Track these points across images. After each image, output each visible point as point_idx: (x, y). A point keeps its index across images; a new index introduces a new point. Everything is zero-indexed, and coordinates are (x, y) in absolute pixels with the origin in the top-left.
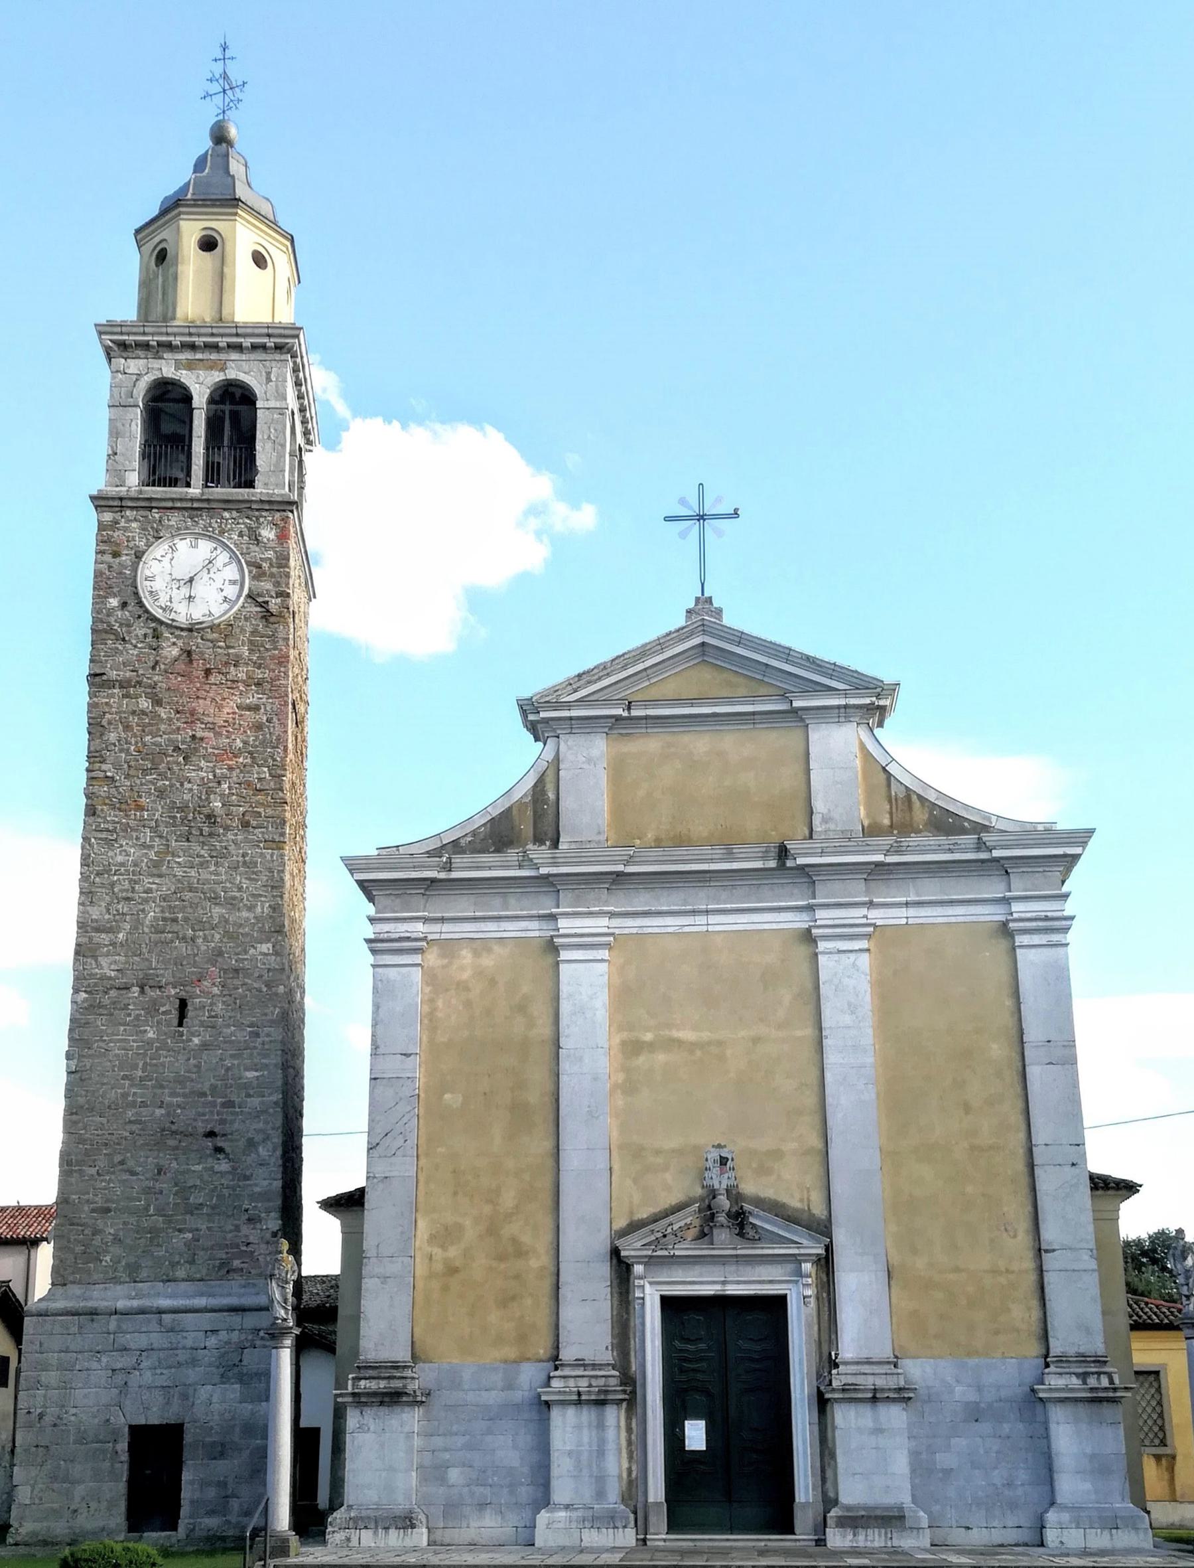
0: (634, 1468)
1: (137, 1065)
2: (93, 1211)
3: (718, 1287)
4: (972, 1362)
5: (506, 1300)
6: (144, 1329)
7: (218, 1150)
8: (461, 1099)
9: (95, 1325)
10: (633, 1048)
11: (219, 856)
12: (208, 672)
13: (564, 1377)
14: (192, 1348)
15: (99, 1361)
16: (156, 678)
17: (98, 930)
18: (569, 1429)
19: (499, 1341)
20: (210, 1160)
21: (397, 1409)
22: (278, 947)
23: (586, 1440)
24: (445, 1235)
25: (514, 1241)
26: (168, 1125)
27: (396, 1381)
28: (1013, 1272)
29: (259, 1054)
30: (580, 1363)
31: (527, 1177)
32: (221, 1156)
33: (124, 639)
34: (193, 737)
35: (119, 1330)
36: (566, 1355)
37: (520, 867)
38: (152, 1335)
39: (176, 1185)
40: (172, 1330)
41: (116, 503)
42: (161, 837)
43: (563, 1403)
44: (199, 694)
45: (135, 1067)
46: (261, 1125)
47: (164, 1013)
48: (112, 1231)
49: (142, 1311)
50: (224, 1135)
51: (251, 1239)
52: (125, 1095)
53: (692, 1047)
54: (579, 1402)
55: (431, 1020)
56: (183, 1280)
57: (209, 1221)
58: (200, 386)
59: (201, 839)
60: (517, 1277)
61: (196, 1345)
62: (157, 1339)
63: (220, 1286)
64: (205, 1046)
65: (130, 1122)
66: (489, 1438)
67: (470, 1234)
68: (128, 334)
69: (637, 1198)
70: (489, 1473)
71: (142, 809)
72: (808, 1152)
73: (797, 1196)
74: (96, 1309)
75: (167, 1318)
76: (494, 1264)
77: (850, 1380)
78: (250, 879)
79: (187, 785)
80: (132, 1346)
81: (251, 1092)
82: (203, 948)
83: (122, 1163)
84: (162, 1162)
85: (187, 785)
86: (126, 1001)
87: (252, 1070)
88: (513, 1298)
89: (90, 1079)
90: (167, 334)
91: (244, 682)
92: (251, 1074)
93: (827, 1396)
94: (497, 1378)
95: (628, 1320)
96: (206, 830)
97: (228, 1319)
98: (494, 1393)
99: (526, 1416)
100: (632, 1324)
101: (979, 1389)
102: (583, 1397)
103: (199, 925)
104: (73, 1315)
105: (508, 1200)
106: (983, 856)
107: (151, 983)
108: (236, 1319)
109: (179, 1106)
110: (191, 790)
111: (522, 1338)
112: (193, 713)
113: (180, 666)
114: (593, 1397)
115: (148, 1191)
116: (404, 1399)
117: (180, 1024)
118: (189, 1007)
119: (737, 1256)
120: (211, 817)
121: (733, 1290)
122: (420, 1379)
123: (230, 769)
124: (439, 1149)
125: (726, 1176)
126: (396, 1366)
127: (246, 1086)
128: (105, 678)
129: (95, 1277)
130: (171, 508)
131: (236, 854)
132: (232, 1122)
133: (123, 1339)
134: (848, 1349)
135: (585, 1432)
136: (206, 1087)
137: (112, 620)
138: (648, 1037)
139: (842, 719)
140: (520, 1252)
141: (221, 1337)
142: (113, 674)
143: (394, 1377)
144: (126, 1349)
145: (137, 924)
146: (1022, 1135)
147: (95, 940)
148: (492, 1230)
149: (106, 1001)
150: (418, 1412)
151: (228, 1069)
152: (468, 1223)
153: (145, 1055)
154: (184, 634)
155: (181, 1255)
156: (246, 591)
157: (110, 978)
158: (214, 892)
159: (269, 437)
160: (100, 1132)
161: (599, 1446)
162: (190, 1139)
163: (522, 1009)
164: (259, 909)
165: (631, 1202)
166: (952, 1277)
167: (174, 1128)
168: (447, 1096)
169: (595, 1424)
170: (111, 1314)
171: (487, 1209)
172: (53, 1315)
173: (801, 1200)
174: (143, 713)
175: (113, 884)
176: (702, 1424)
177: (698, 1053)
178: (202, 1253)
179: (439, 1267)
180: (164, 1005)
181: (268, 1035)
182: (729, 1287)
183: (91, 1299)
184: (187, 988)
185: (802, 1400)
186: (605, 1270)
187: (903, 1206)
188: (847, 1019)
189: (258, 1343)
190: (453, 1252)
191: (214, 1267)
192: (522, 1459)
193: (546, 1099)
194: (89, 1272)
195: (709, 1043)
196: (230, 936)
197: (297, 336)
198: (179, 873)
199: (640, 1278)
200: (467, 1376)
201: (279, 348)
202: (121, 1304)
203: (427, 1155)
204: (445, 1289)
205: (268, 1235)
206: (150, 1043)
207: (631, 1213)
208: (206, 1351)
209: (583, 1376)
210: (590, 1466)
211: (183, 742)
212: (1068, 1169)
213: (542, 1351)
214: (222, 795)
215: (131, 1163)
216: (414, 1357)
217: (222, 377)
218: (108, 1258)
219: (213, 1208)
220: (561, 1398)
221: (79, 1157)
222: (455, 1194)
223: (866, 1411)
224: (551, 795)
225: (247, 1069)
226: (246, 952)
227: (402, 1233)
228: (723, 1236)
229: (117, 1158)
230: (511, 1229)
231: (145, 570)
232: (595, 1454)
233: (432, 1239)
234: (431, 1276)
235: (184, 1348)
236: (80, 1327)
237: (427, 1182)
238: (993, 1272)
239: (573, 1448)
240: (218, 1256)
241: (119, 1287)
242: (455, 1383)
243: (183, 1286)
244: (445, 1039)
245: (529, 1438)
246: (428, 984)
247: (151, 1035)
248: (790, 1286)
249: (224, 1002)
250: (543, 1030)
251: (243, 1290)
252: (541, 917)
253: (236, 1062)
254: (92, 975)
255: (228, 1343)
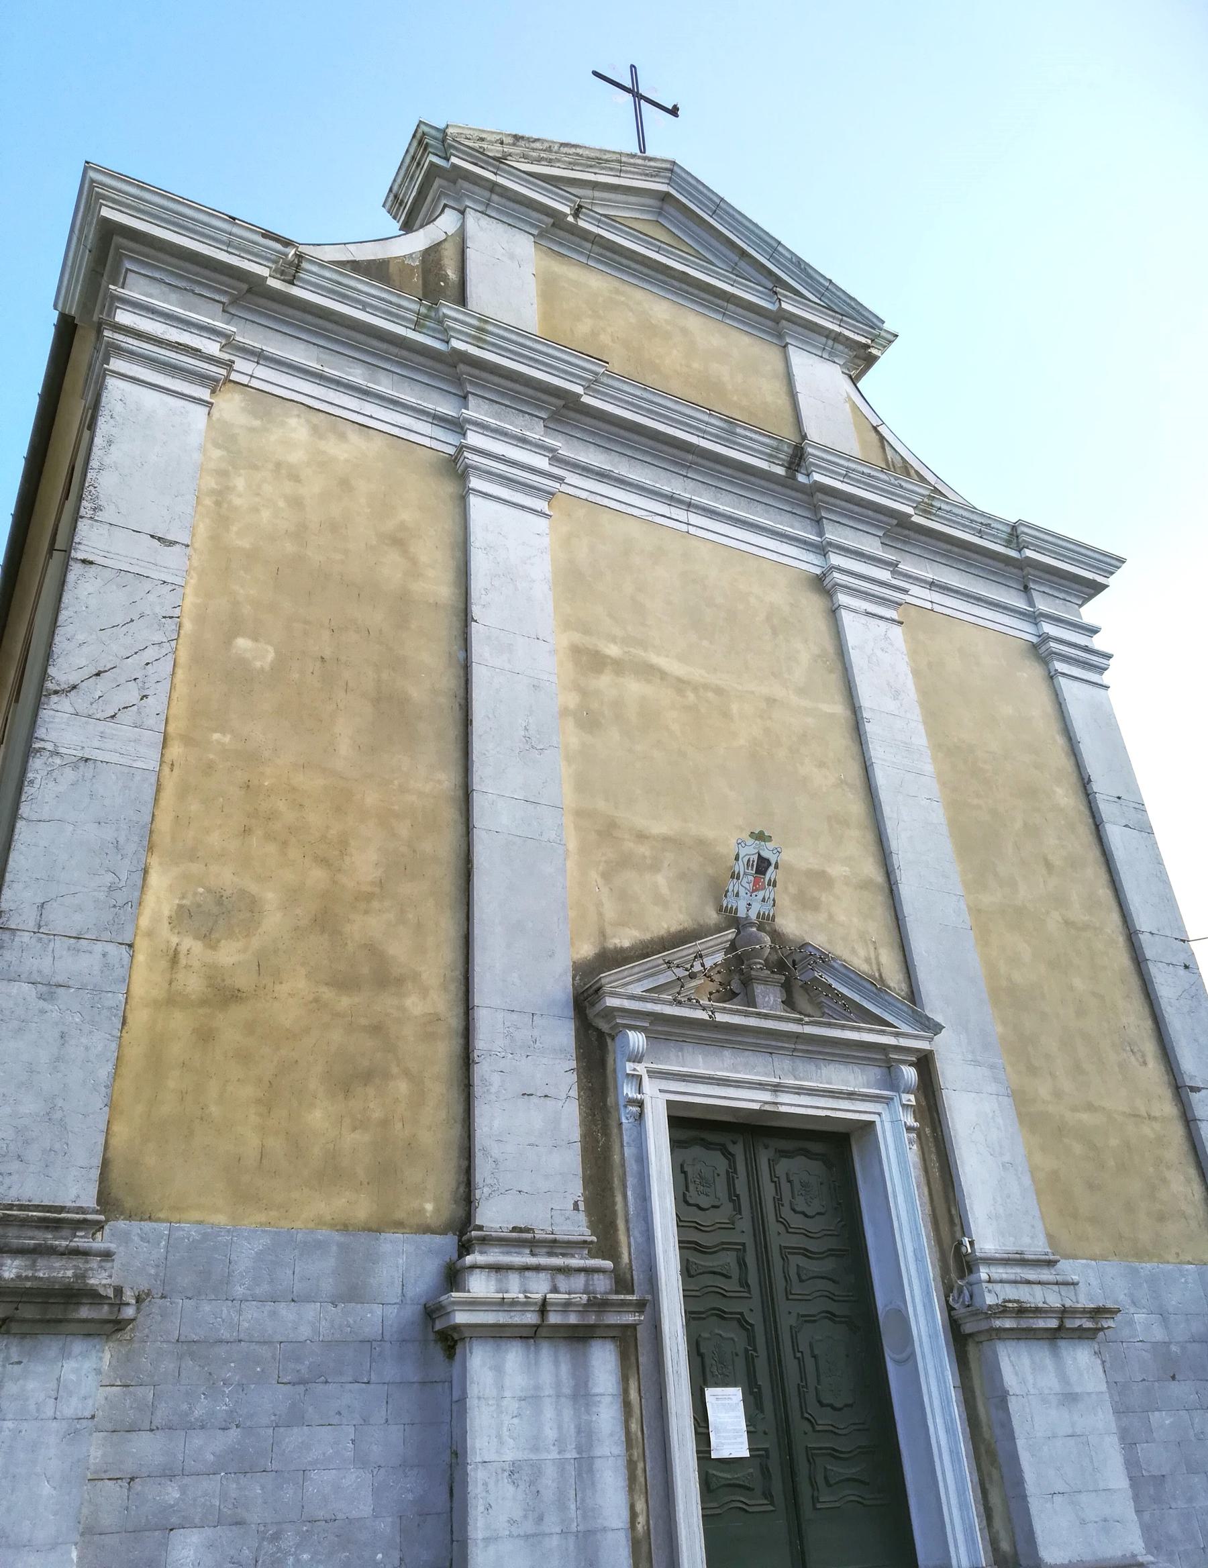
0: (640, 1506)
3: (766, 1096)
4: (1147, 1267)
5: (351, 1079)
8: (271, 656)
10: (589, 661)
13: (497, 1268)
18: (512, 1405)
19: (332, 1173)
21: (51, 1347)
23: (550, 1433)
24: (210, 915)
25: (372, 950)
27: (57, 1263)
28: (1155, 1118)
30: (522, 1239)
31: (403, 830)
36: (493, 1214)
37: (417, 326)
43: (498, 1334)
53: (681, 685)
54: (531, 1335)
55: (218, 504)
60: (377, 1029)
66: (294, 1437)
67: (274, 922)
69: (610, 911)
70: (290, 1539)
72: (865, 885)
73: (862, 953)
76: (327, 994)
77: (1011, 1292)
88: (367, 1077)
93: (968, 1328)
94: (322, 1269)
95: (607, 1149)
98: (310, 1311)
99: (390, 1371)
100: (616, 1158)
101: (1164, 1316)
102: (554, 1318)
105: (364, 864)
106: (1013, 554)
111: (384, 1174)
114: (573, 1319)
116: (85, 1312)
119: (797, 1037)
121: (791, 1104)
122: (127, 1257)
124: (216, 736)
125: (761, 894)
126: (54, 1220)
134: (986, 1236)
135: (549, 1413)
138: (613, 650)
139: (826, 355)
140: (386, 978)
143: (52, 1251)
146: (1115, 917)
148: (325, 921)
150: (104, 1356)
152: (270, 897)
161: (579, 1449)
163: (398, 541)
165: (600, 915)
166: (1085, 1117)
168: (242, 643)
169: (567, 1390)
171: (317, 876)
173: (868, 960)
176: (735, 1395)
177: (691, 697)
179: (192, 984)
182: (784, 1098)
185: (933, 1336)
186: (564, 1035)
187: (1008, 997)
188: (891, 706)
190: (229, 953)
192: (376, 1492)
193: (442, 700)
195: (706, 687)
199: (638, 1059)
200: (245, 1255)
203: (188, 740)
204: (205, 1036)
207: (603, 934)
209: (537, 1268)
210: (562, 1506)
212: (1182, 971)
213: (429, 1207)
216: (106, 1200)
220: (502, 1318)
222: (247, 831)
223: (1041, 1353)
224: (452, 274)
227: (111, 889)
228: (769, 997)
230: (366, 926)
232: (571, 1470)
233: (183, 917)
234: (172, 1000)
237: (183, 792)
238: (1135, 1116)
239: (520, 1455)
242: (213, 1282)
244: (245, 543)
245: (395, 1433)
246: (217, 445)
248: (878, 1107)
250: (437, 585)
252: (439, 420)
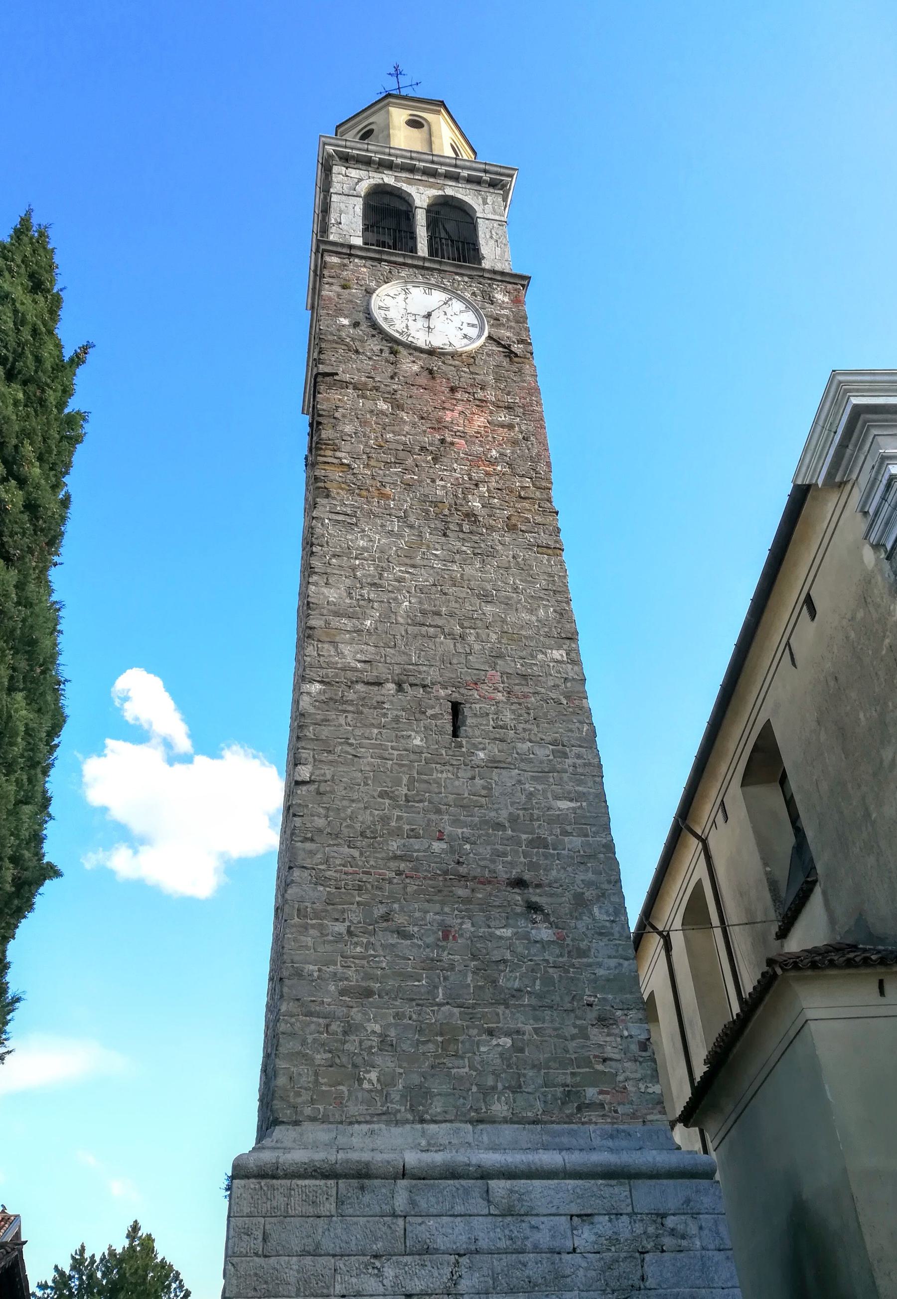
1: (401, 780)
2: (343, 992)
6: (459, 1209)
7: (533, 907)
9: (367, 1198)
11: (486, 555)
12: (453, 390)
14: (552, 1251)
15: (380, 1274)
16: (395, 387)
17: (337, 614)
20: (522, 922)
22: (573, 655)
26: (453, 865)
29: (571, 779)
32: (539, 918)
33: (357, 352)
34: (443, 441)
35: (414, 1211)
38: (475, 1221)
39: (474, 957)
40: (508, 1212)
41: (345, 250)
42: (411, 527)
44: (446, 405)
45: (398, 783)
46: (590, 876)
47: (434, 717)
48: (377, 1028)
49: (452, 1173)
50: (538, 886)
51: (609, 1052)
52: (385, 820)
56: (505, 1121)
57: (536, 1019)
58: (422, 196)
59: (461, 535)
61: (556, 1244)
62: (486, 1232)
63: (571, 1133)
64: (494, 764)
65: (395, 857)
68: (352, 149)
71: (388, 497)
74: (367, 1164)
75: (499, 1186)
78: (525, 581)
79: (438, 482)
80: (441, 1243)
81: (569, 828)
82: (477, 647)
83: (386, 917)
84: (449, 921)
85: (438, 482)
86: (380, 698)
87: (565, 798)
89: (332, 792)
90: (390, 155)
91: (493, 403)
92: (564, 805)
96: (466, 528)
97: (607, 1192)
103: (469, 621)
104: (326, 1176)
107: (412, 680)
108: (618, 1191)
109: (466, 840)
110: (444, 487)
112: (439, 421)
113: (423, 380)
115: (431, 964)
117: (455, 734)
118: (467, 712)
120: (471, 516)
123: (487, 474)
127: (560, 819)
128: (336, 378)
129: (354, 1109)
130: (404, 264)
131: (505, 555)
132: (547, 870)
133: (428, 1229)
136: (503, 816)
137: (343, 334)
141: (599, 1229)
142: (347, 377)
144: (428, 1251)
145: (388, 615)
147: (332, 624)
149: (351, 695)
151: (531, 795)
153: (410, 767)
154: (424, 356)
155: (496, 1075)
156: (486, 334)
157: (355, 670)
158: (484, 590)
159: (491, 237)
160: (350, 870)
162: (489, 888)
164: (541, 612)
167: (463, 870)
170: (395, 1178)
172: (286, 1176)
174: (382, 413)
175: (354, 569)
178: (530, 1073)
180: (433, 707)
181: (579, 756)
183: (352, 1148)
184: (462, 690)
189: (668, 1242)
191: (555, 1099)
194: (339, 1101)
196: (514, 638)
197: (511, 176)
198: (438, 565)
201: (493, 184)
202: (412, 1158)
205: (634, 1048)
206: (417, 752)
208: (577, 1258)
211: (431, 444)
214: (481, 497)
215: (400, 919)
217: (440, 193)
218: (373, 1076)
219: (540, 996)
221: (318, 906)
225: (557, 798)
226: (533, 657)
229: (379, 911)
231: (375, 302)
235: (537, 1249)
236: (340, 1202)
240: (560, 1079)
241: (396, 1131)
243: (508, 1132)
247: (417, 742)
249: (513, 712)
251: (610, 1143)
253: (540, 787)
254: (330, 665)
255: (614, 1240)
